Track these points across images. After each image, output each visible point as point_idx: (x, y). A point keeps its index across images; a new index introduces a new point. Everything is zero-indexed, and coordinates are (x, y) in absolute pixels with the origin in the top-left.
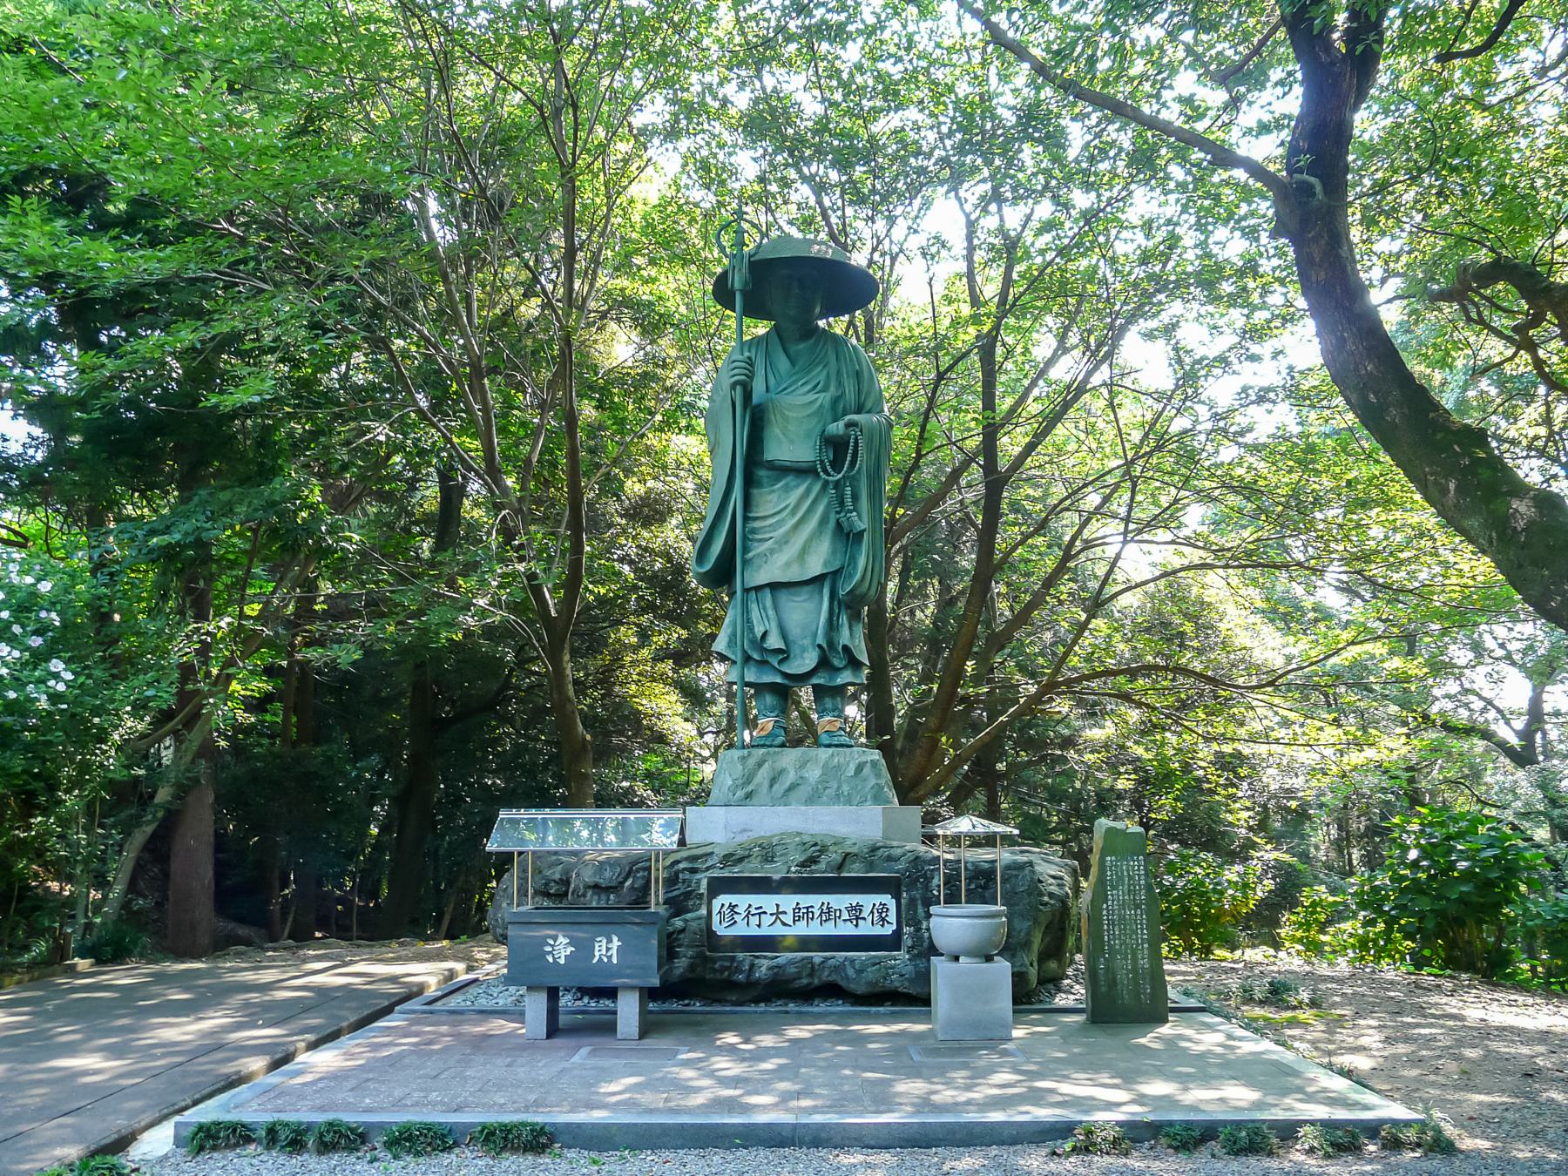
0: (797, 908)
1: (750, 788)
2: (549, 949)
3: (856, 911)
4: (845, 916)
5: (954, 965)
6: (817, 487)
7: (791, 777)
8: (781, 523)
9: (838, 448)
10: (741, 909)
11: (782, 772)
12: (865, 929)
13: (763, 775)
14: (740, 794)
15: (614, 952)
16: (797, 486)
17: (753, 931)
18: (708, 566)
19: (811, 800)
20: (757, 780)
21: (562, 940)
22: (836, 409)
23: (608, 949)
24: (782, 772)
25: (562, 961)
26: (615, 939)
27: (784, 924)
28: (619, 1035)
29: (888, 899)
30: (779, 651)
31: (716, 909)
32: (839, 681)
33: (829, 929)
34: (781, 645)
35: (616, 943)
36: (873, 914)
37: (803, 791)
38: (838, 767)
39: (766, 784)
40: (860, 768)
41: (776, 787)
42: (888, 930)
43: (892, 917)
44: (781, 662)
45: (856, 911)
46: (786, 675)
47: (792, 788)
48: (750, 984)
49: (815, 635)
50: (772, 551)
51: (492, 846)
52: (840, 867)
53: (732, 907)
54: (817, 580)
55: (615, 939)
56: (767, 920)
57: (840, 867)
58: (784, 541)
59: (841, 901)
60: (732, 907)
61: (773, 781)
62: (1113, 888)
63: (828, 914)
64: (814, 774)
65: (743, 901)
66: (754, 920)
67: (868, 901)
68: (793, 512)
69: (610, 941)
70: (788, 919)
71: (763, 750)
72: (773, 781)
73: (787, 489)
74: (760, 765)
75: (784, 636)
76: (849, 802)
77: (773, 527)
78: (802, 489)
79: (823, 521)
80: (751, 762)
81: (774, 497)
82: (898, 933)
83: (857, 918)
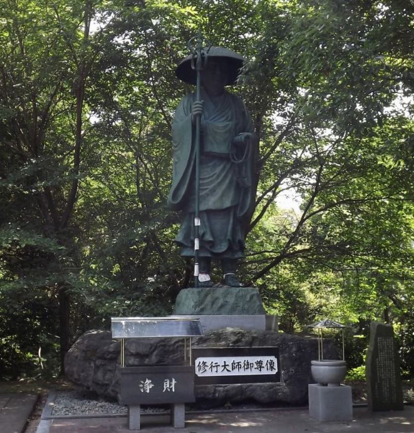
0: (233, 363)
1: (202, 306)
2: (141, 386)
3: (260, 363)
4: (255, 366)
5: (325, 387)
6: (228, 166)
7: (221, 301)
8: (211, 182)
9: (239, 148)
10: (208, 364)
11: (217, 298)
12: (265, 372)
13: (209, 298)
14: (198, 309)
15: (173, 386)
16: (220, 165)
17: (214, 374)
18: (176, 202)
19: (232, 311)
20: (206, 302)
21: (148, 381)
22: (237, 130)
23: (170, 385)
24: (217, 298)
25: (148, 391)
26: (174, 380)
27: (228, 370)
28: (175, 427)
29: (199, 374)
30: (210, 242)
31: (197, 364)
32: (236, 256)
33: (248, 373)
34: (211, 239)
35: (174, 382)
36: (265, 365)
37: (228, 307)
38: (242, 297)
39: (210, 304)
40: (252, 297)
41: (214, 306)
42: (274, 372)
43: (276, 366)
44: (211, 247)
45: (260, 363)
46: (212, 253)
47: (222, 306)
48: (214, 400)
49: (226, 235)
50: (207, 195)
51: (358, 321)
52: (251, 344)
53: (204, 363)
54: (228, 210)
55: (174, 380)
56: (220, 369)
57: (251, 344)
58: (213, 191)
59: (253, 360)
60: (204, 363)
61: (213, 303)
62: (381, 351)
63: (248, 365)
64: (231, 300)
65: (209, 360)
66: (214, 369)
67: (265, 359)
68: (218, 176)
69: (171, 381)
70: (230, 368)
71: (208, 288)
72: (213, 303)
73: (215, 166)
74: (206, 296)
75: (213, 235)
76: (248, 312)
77: (208, 184)
78: (221, 167)
79: (231, 182)
80: (203, 294)
81: (209, 169)
82: (278, 373)
83: (261, 367)
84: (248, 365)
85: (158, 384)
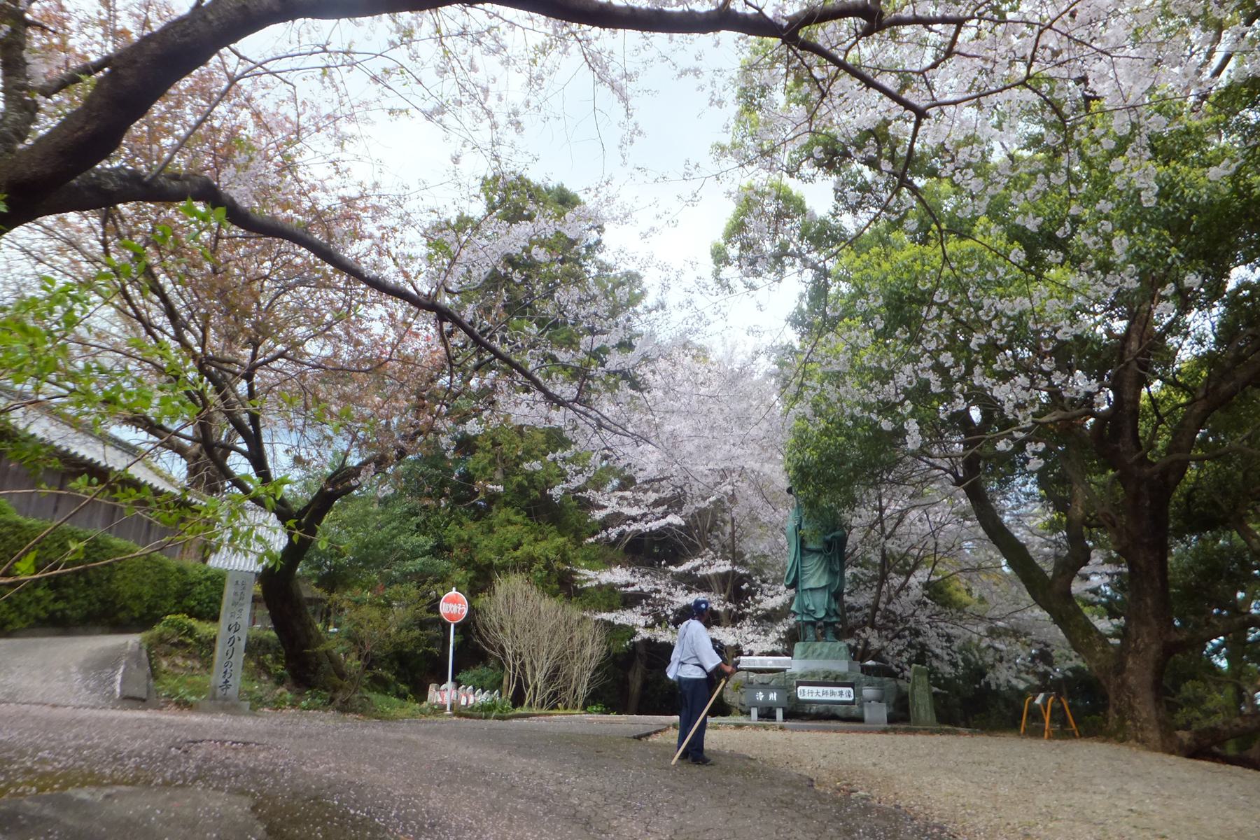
12: (844, 698)
13: (810, 650)
42: (851, 699)
67: (845, 690)
84: (833, 693)
85: (766, 696)
